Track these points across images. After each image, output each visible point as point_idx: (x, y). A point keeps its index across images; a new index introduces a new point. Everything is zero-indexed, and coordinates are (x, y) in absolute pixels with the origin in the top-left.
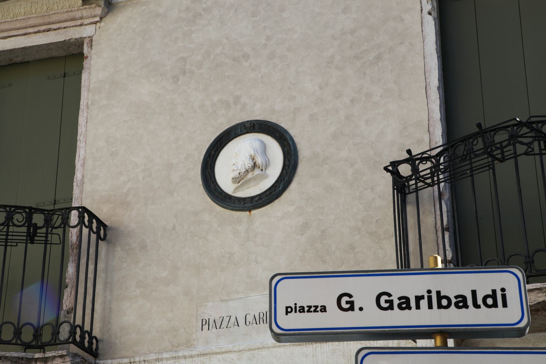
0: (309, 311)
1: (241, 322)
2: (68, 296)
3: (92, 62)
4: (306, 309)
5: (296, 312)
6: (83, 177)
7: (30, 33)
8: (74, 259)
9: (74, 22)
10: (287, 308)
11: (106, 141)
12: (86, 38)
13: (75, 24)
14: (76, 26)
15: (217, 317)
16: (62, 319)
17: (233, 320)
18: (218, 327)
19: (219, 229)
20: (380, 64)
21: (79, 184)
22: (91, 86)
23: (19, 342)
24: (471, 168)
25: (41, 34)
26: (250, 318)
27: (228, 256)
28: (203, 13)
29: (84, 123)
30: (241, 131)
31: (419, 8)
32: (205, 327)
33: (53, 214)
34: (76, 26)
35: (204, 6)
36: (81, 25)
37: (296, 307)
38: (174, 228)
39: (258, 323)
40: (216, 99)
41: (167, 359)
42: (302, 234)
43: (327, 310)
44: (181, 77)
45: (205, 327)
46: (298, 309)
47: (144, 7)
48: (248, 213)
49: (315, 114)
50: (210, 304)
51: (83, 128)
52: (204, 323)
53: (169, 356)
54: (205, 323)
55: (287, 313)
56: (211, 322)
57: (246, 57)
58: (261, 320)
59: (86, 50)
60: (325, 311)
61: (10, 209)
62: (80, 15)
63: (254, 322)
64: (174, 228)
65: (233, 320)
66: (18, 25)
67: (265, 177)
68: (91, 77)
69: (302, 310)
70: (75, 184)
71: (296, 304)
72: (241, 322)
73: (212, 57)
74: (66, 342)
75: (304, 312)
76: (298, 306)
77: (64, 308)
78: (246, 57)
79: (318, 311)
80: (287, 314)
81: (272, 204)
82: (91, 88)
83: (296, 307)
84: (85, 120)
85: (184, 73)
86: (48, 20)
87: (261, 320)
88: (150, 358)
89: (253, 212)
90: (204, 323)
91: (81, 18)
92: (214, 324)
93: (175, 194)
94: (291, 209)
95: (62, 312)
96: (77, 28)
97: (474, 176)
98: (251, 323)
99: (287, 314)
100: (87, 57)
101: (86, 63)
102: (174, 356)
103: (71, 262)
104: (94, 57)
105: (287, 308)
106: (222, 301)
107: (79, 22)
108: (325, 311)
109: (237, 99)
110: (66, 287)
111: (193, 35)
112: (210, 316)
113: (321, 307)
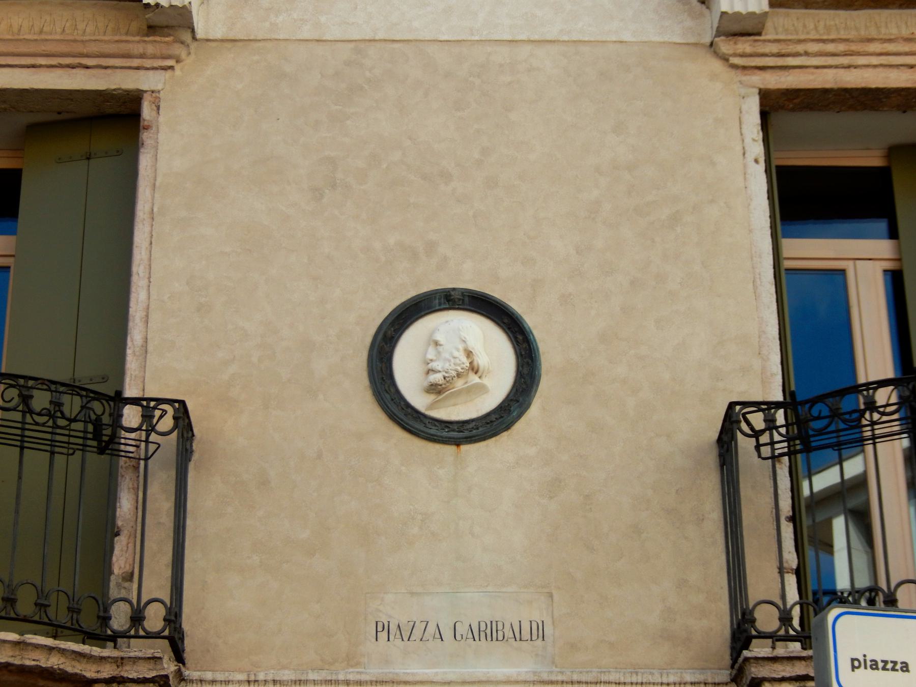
0: (884, 669)
1: (447, 634)
2: (122, 550)
3: (161, 137)
4: (881, 665)
5: (866, 668)
6: (146, 340)
7: (40, 66)
8: (131, 486)
9: (125, 60)
10: (853, 660)
11: (187, 284)
12: (146, 91)
13: (128, 64)
14: (130, 68)
15: (403, 621)
16: (114, 593)
17: (432, 628)
18: (406, 639)
19: (403, 468)
20: (679, 229)
21: (137, 353)
22: (159, 180)
23: (142, 633)
24: (873, 435)
25: (59, 72)
26: (462, 629)
27: (420, 517)
28: (366, 87)
29: (145, 244)
30: (440, 304)
31: (739, 148)
32: (383, 635)
33: (155, 408)
34: (130, 68)
35: (368, 74)
36: (138, 68)
37: (865, 661)
38: (320, 456)
39: (477, 638)
40: (392, 241)
41: (314, 682)
42: (551, 498)
43: (910, 668)
44: (327, 191)
45: (383, 635)
46: (869, 663)
47: (256, 58)
48: (454, 448)
49: (570, 294)
50: (389, 597)
51: (143, 253)
52: (380, 629)
53: (320, 678)
54: (382, 628)
55: (854, 668)
56: (393, 628)
57: (446, 177)
58: (483, 634)
59: (147, 112)
60: (908, 671)
61: (148, 404)
62: (141, 51)
63: (470, 635)
64: (320, 456)
65: (432, 628)
66: (23, 49)
67: (481, 389)
68: (158, 164)
69: (874, 665)
70: (129, 352)
71: (865, 656)
72: (447, 634)
73: (384, 166)
74: (157, 636)
75: (877, 669)
76: (868, 658)
77: (116, 570)
78: (446, 177)
79: (897, 670)
80: (853, 670)
81: (498, 437)
82: (157, 184)
83: (865, 661)
84: (148, 240)
85: (334, 186)
86: (80, 48)
87: (483, 634)
88: (285, 678)
89: (464, 448)
90: (380, 629)
91: (142, 56)
92: (398, 632)
93: (321, 397)
94: (532, 451)
95: (113, 578)
96: (131, 72)
97: (878, 445)
98: (464, 637)
99: (853, 670)
100: (147, 128)
101: (145, 136)
102: (329, 678)
103: (126, 491)
104: (163, 128)
105: (853, 660)
106: (412, 594)
107: (136, 62)
108: (908, 671)
109: (431, 248)
110: (117, 534)
111: (348, 122)
112: (390, 617)
113: (902, 663)
